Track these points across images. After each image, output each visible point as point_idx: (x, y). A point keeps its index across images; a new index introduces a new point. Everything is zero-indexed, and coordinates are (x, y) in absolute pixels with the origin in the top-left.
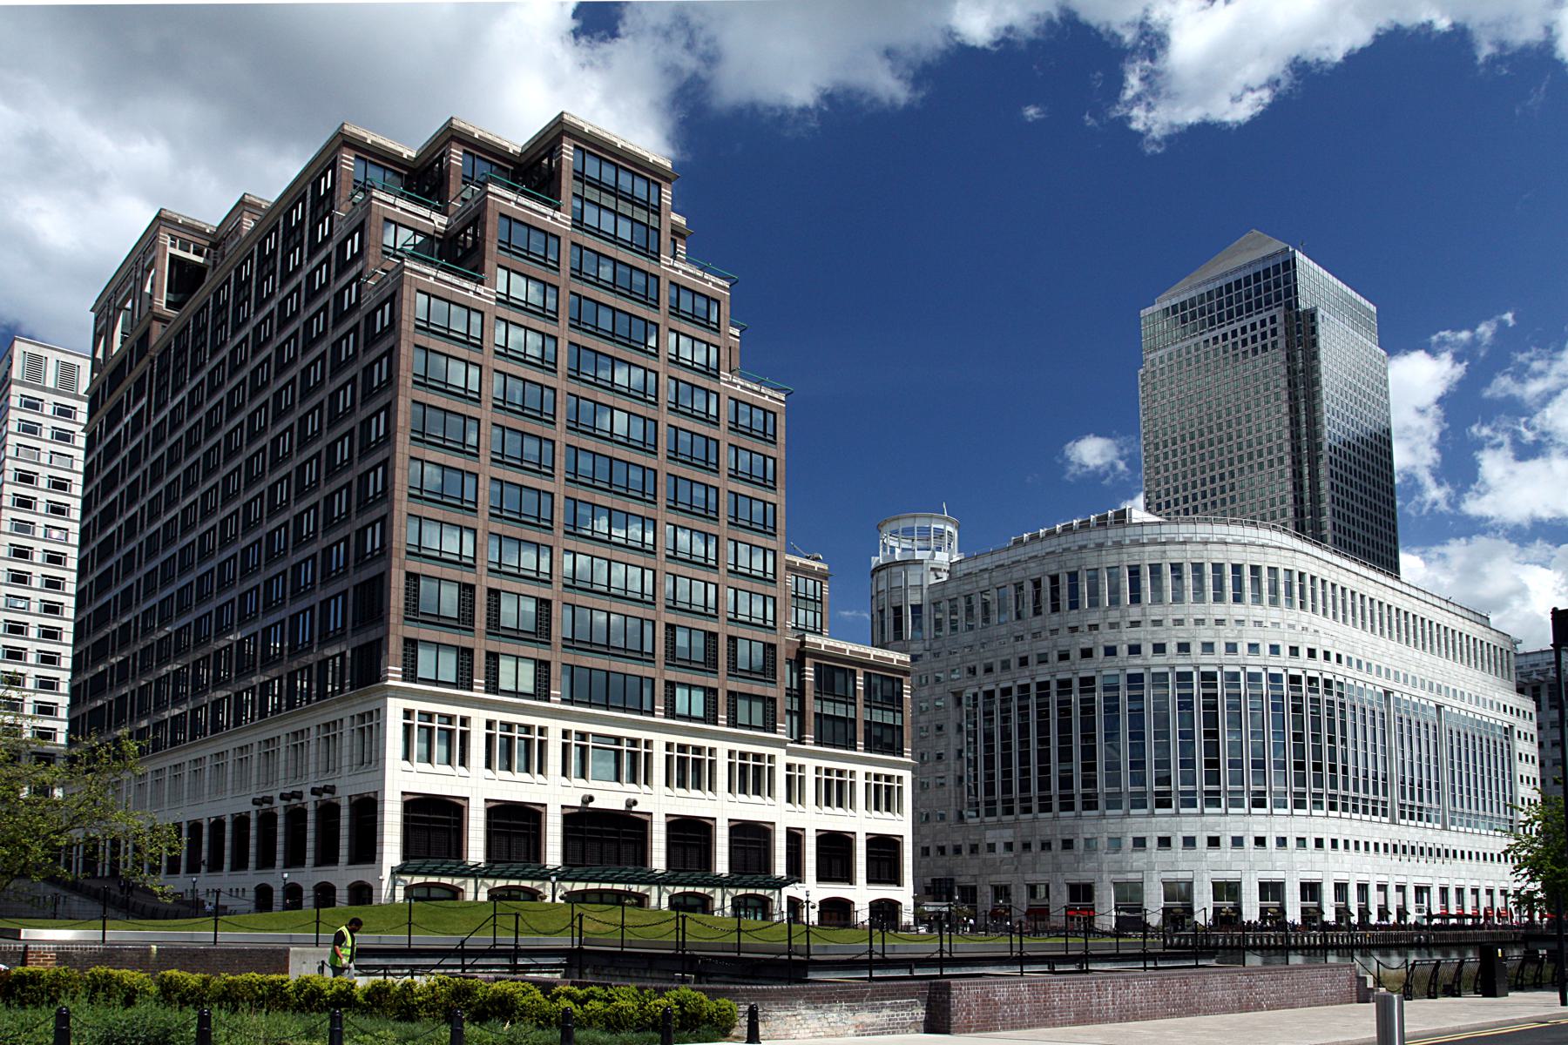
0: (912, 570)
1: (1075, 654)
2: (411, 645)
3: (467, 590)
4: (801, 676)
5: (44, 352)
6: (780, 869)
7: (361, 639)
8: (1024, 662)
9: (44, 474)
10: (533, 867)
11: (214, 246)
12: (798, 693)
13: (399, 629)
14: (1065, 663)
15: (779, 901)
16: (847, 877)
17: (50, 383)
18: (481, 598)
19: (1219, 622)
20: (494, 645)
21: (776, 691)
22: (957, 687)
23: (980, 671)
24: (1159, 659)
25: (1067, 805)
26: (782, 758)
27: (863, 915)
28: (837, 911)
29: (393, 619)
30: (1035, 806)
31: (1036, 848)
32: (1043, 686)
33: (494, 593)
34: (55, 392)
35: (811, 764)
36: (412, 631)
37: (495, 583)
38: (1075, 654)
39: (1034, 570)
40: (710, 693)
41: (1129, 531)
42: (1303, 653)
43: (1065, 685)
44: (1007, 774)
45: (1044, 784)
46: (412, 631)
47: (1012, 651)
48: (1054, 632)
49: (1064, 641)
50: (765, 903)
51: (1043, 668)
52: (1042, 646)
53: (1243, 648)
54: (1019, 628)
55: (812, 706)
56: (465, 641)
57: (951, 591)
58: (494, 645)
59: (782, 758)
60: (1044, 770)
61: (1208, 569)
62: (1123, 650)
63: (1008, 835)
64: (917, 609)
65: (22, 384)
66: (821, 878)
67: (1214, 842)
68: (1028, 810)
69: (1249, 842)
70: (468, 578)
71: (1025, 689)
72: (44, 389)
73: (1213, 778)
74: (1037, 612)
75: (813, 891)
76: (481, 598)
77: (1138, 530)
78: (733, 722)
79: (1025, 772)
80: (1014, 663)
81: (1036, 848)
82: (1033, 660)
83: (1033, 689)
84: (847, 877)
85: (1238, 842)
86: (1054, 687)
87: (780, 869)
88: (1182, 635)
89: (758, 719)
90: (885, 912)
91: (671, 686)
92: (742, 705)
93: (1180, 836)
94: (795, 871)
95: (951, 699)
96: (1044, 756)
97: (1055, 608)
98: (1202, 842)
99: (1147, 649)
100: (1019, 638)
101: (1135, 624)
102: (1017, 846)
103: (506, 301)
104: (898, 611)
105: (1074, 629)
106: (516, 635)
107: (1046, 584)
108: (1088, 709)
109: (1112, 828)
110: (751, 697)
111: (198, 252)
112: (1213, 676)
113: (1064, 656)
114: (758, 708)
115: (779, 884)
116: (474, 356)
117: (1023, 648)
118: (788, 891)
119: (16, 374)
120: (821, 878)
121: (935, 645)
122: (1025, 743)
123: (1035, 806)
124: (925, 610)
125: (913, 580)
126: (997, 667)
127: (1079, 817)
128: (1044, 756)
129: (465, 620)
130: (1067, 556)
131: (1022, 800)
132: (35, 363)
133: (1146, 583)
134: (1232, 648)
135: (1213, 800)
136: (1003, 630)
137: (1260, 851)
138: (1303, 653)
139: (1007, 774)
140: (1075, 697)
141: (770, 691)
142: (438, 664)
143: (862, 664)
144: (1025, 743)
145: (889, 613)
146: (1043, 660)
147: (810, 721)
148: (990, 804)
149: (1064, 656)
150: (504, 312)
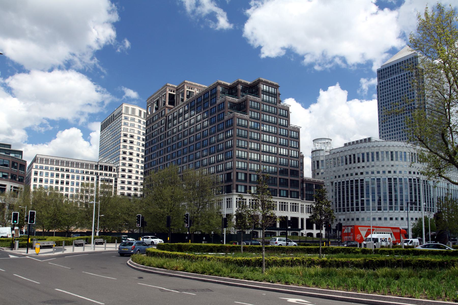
0: (321, 152)
1: (359, 174)
2: (237, 186)
3: (246, 174)
4: (303, 186)
5: (129, 106)
6: (300, 227)
7: (227, 184)
8: (347, 175)
9: (129, 134)
10: (274, 228)
11: (177, 90)
12: (302, 189)
13: (235, 183)
14: (357, 176)
15: (300, 234)
16: (312, 228)
17: (130, 113)
18: (248, 176)
19: (392, 166)
20: (250, 185)
21: (299, 190)
22: (332, 180)
23: (337, 177)
24: (378, 175)
25: (357, 210)
26: (300, 203)
27: (315, 236)
28: (310, 235)
29: (234, 181)
30: (350, 210)
31: (350, 220)
32: (352, 181)
33: (250, 175)
34: (131, 115)
35: (305, 204)
36: (237, 183)
37: (250, 173)
38: (359, 174)
39: (350, 153)
40: (287, 191)
41: (371, 143)
42: (412, 173)
43: (357, 181)
44: (344, 202)
45: (352, 205)
46: (237, 183)
47: (345, 172)
48: (354, 168)
49: (357, 170)
50: (297, 234)
51: (352, 177)
52: (351, 171)
53: (398, 172)
54: (346, 167)
55: (305, 192)
56: (246, 184)
57: (330, 157)
58: (250, 185)
59: (300, 203)
60: (352, 201)
61: (390, 153)
62: (370, 173)
63: (344, 217)
64: (322, 161)
65: (124, 114)
66: (307, 228)
67: (391, 219)
68: (348, 211)
69: (400, 219)
70: (246, 172)
71: (348, 182)
72: (129, 115)
73: (391, 203)
74: (350, 163)
75: (305, 231)
76: (248, 176)
77: (374, 143)
78: (291, 197)
79: (348, 202)
80: (345, 175)
81: (350, 220)
82: (349, 175)
83: (350, 182)
84: (312, 228)
85: (396, 219)
86: (354, 181)
87: (300, 227)
88: (383, 169)
89: (295, 196)
90: (319, 235)
91: (280, 190)
92: (293, 193)
93: (383, 217)
94: (302, 228)
95: (330, 184)
96: (352, 198)
97: (354, 162)
98: (388, 219)
99: (375, 172)
100: (346, 169)
101: (373, 166)
102: (346, 220)
103: (251, 117)
104: (318, 162)
105: (359, 167)
106: (254, 182)
107: (352, 156)
108: (362, 187)
109: (368, 215)
110: (294, 191)
111: (174, 92)
112: (391, 179)
113: (356, 174)
114: (295, 193)
115: (300, 230)
116: (246, 129)
117: (347, 172)
118: (302, 231)
119: (123, 111)
120: (307, 228)
121: (327, 170)
122: (348, 195)
123: (350, 210)
124: (324, 161)
125: (322, 154)
126: (341, 176)
127: (360, 213)
128: (352, 198)
129: (246, 180)
130: (357, 150)
131: (347, 208)
132: (127, 108)
133: (375, 156)
134: (395, 172)
135: (391, 208)
136: (343, 167)
137: (402, 221)
138: (412, 173)
139: (344, 202)
140: (359, 184)
141: (298, 190)
142: (241, 189)
143: (315, 182)
144: (348, 195)
145: (316, 162)
146: (352, 175)
147: (305, 195)
148: (340, 209)
149: (356, 174)
150: (251, 120)
